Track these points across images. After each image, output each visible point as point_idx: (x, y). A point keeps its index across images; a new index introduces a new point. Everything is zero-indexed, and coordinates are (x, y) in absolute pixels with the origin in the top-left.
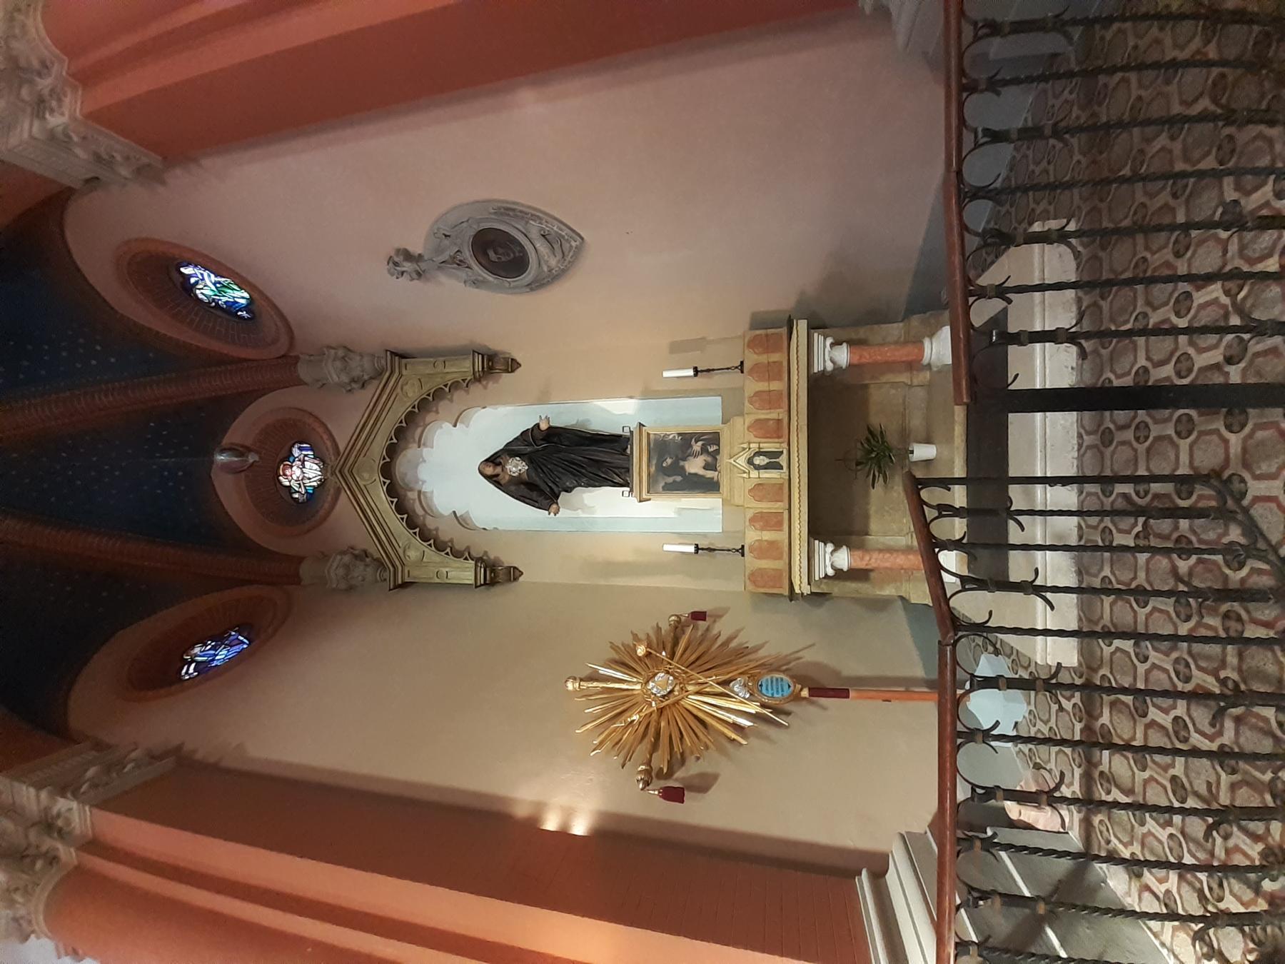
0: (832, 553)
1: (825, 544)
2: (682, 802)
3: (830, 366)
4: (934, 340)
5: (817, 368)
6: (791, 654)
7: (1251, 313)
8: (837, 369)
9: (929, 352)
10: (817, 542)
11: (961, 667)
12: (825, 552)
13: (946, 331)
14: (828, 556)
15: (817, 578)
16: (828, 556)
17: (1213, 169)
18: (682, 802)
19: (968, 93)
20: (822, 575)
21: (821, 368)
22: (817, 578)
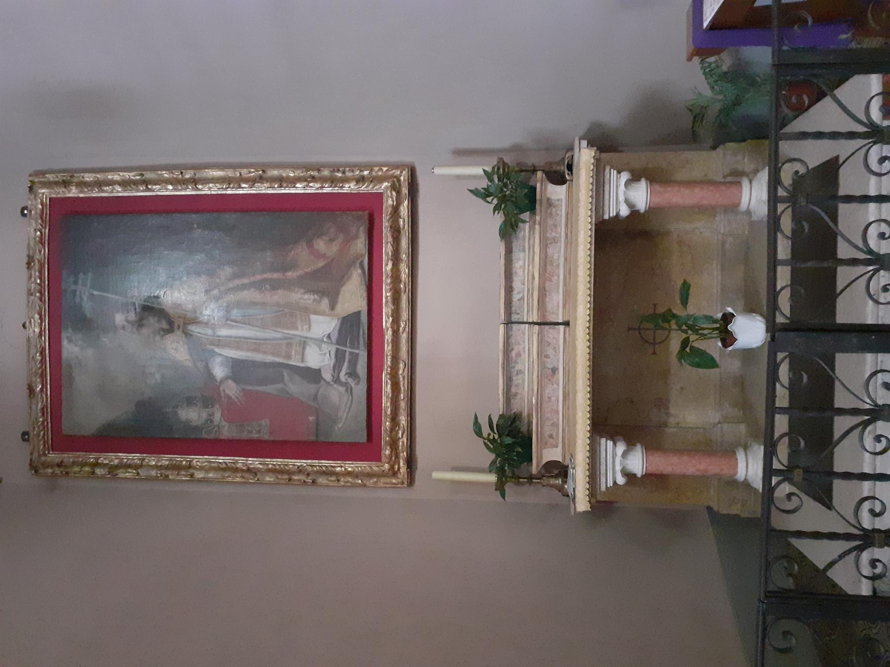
0: (625, 455)
1: (615, 444)
2: (737, 340)
3: (624, 211)
4: (754, 183)
5: (610, 212)
6: (643, 471)
7: (778, 265)
8: (634, 213)
9: (747, 199)
10: (603, 440)
11: (775, 505)
12: (614, 455)
13: (767, 168)
14: (618, 459)
15: (603, 488)
16: (618, 459)
17: (559, 462)
18: (737, 340)
19: (780, 478)
20: (610, 483)
21: (613, 214)
22: (603, 488)
